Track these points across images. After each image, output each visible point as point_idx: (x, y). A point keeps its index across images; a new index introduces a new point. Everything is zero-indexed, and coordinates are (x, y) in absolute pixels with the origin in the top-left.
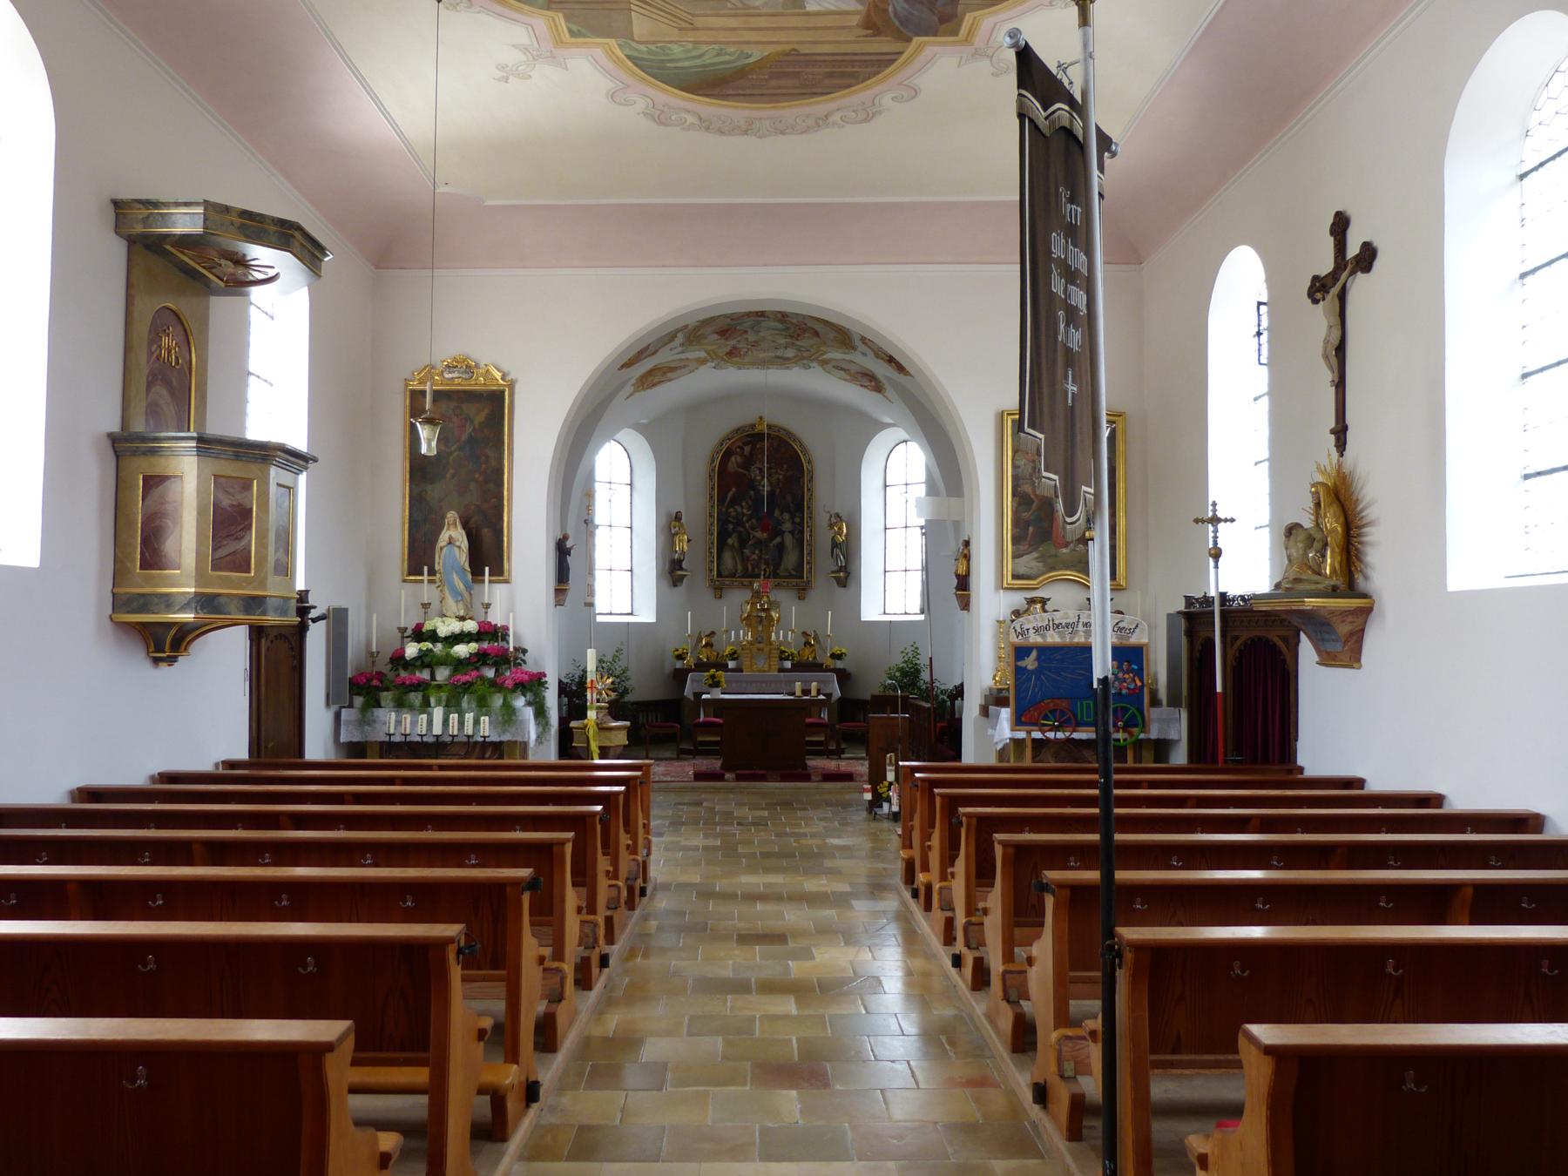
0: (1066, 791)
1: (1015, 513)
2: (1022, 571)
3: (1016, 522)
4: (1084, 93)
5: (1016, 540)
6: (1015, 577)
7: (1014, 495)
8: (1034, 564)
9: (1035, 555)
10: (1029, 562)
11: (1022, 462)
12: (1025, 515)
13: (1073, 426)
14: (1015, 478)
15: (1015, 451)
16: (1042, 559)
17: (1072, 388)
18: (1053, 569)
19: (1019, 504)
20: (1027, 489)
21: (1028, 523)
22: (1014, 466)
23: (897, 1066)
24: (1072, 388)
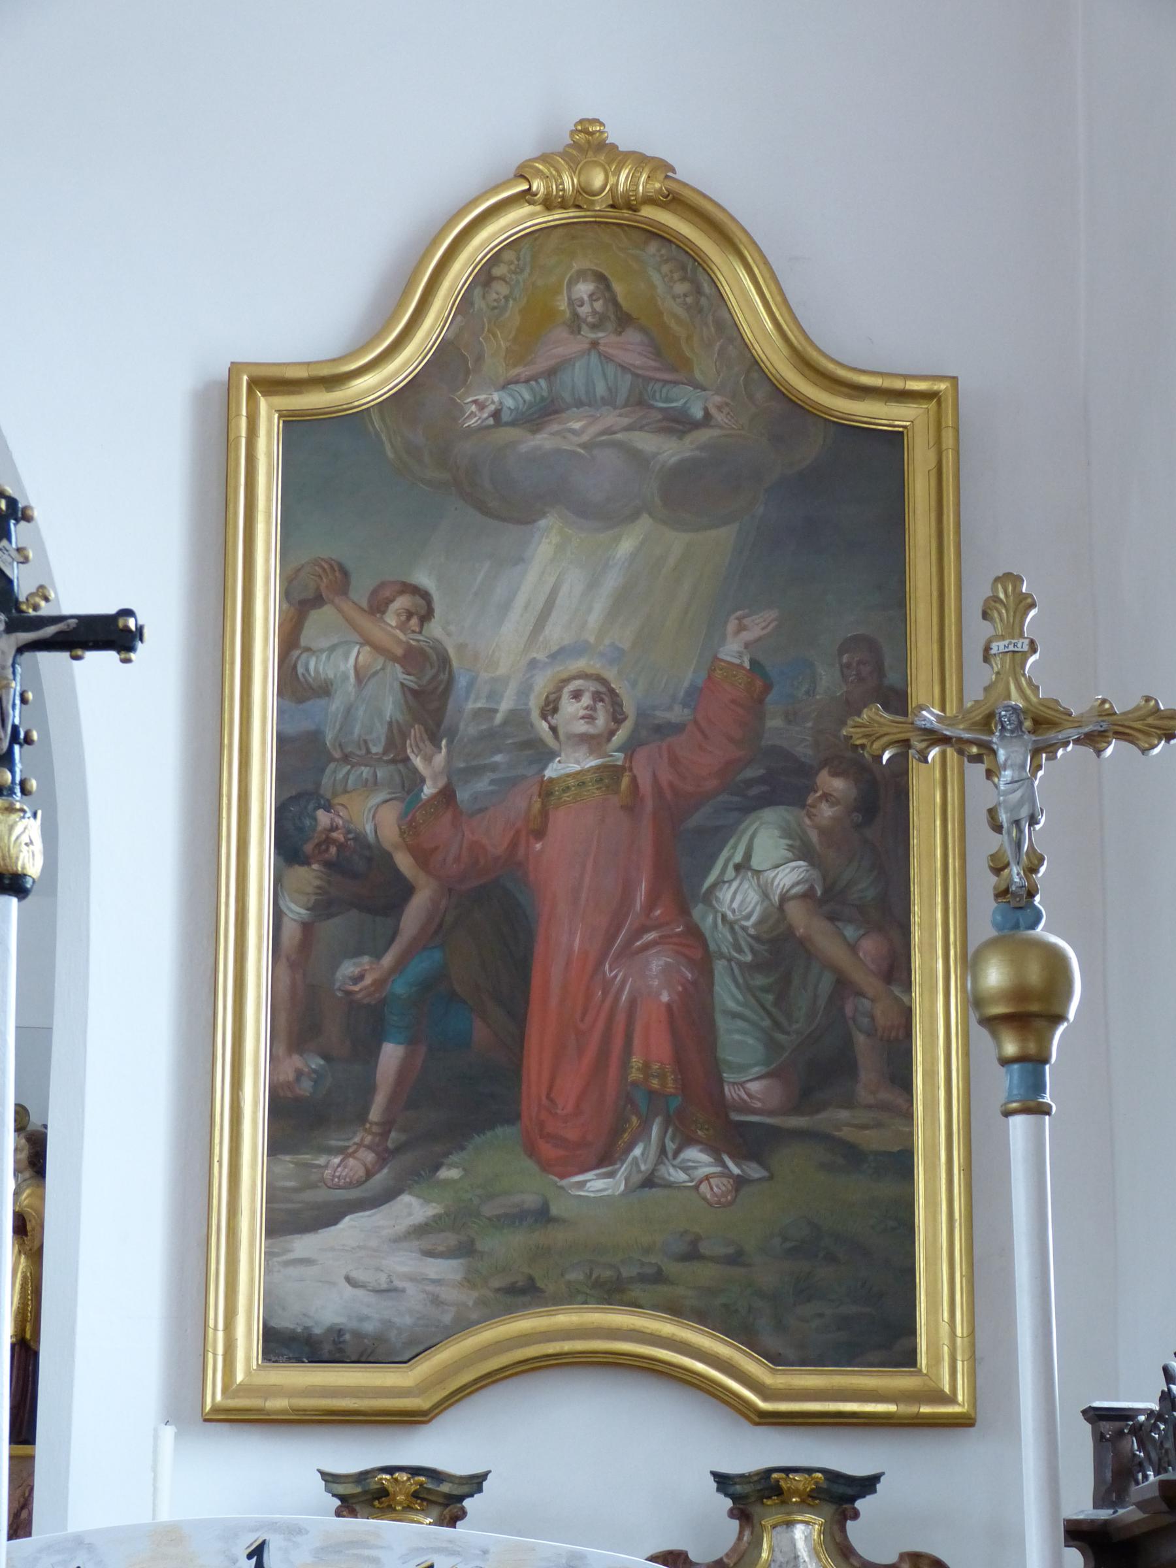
0: (700, 1367)
1: (296, 958)
2: (328, 1307)
3: (303, 1017)
4: (564, 437)
5: (295, 1120)
6: (281, 1344)
7: (289, 848)
8: (404, 1263)
9: (412, 1209)
10: (373, 1259)
11: (338, 661)
12: (357, 973)
13: (959, 493)
14: (300, 757)
15: (300, 604)
16: (454, 1233)
17: (886, 756)
18: (523, 1293)
19: (324, 907)
20: (372, 815)
21: (368, 1023)
22: (294, 686)
23: (324, 643)
24: (886, 756)
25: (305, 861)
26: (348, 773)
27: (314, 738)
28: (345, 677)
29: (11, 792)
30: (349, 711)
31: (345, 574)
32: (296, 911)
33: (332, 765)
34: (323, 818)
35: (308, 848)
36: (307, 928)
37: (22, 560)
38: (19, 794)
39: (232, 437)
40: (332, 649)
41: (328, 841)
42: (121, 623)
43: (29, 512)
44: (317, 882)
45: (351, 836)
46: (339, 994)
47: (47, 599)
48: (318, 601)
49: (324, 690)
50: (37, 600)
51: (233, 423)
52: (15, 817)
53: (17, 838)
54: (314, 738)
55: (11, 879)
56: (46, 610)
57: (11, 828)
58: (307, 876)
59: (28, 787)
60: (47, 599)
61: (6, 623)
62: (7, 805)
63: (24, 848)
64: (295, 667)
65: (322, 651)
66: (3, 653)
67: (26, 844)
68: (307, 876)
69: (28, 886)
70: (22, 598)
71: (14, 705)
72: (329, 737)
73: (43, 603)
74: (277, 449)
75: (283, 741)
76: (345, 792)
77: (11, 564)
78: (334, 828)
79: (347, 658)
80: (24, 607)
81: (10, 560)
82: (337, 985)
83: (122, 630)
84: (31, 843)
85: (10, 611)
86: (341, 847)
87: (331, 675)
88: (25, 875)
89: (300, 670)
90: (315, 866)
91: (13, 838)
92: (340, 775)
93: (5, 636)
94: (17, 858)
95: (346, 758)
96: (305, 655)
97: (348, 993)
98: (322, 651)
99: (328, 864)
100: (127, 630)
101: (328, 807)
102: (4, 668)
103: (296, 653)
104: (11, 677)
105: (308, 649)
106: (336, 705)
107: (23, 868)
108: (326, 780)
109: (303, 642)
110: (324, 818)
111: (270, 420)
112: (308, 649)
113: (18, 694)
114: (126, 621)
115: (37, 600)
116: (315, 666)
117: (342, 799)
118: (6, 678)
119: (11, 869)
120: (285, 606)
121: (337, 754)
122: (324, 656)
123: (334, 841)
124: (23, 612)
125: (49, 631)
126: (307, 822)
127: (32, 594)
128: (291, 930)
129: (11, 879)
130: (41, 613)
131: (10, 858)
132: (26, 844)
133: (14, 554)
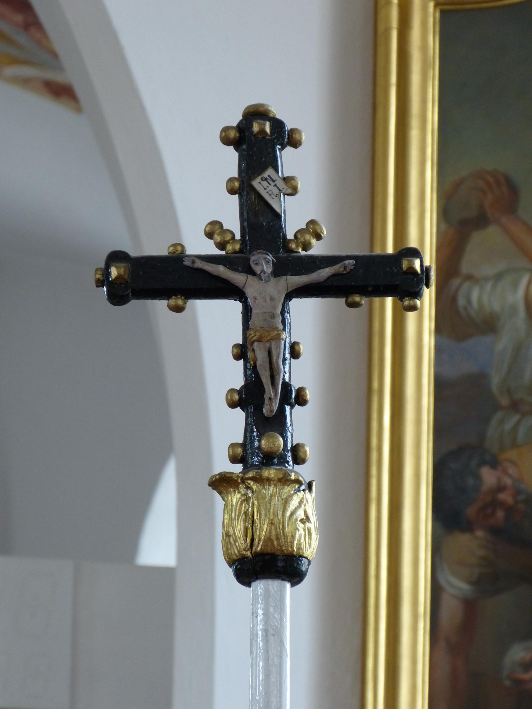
7: (448, 514)
19: (489, 581)
23: (488, 270)
25: (467, 527)
26: (518, 424)
27: (477, 382)
28: (514, 310)
29: (283, 461)
30: (518, 350)
31: (513, 190)
32: (457, 585)
33: (499, 415)
34: (489, 477)
35: (471, 511)
36: (470, 606)
37: (289, 191)
38: (291, 463)
39: (381, 28)
40: (498, 277)
41: (495, 504)
42: (405, 265)
43: (296, 136)
44: (481, 552)
45: (521, 497)
46: (507, 683)
47: (318, 237)
48: (481, 221)
49: (489, 325)
50: (308, 237)
51: (382, 14)
52: (288, 489)
53: (292, 514)
54: (477, 382)
55: (285, 561)
56: (317, 249)
57: (286, 502)
58: (469, 545)
59: (301, 454)
60: (318, 237)
61: (274, 264)
62: (281, 476)
63: (301, 526)
64: (454, 300)
65: (486, 279)
66: (272, 299)
67: (302, 521)
68: (469, 545)
69: (304, 569)
70: (290, 235)
71: (284, 359)
72: (495, 381)
73: (314, 241)
74: (433, 43)
75: (441, 386)
76: (515, 445)
77: (278, 196)
78: (500, 488)
79: (515, 285)
80: (293, 246)
81: (276, 191)
82: (505, 673)
83: (405, 273)
84: (308, 519)
85: (279, 252)
86: (509, 510)
87: (497, 307)
88: (301, 556)
89: (461, 302)
90: (480, 533)
91: (288, 514)
92: (508, 426)
93: (273, 280)
94: (293, 537)
95: (515, 406)
96: (466, 285)
97: (519, 682)
98: (486, 279)
99: (495, 532)
100: (412, 271)
101: (494, 464)
102: (273, 316)
103: (455, 282)
104: (281, 327)
105: (470, 278)
106: (503, 343)
107: (299, 548)
108: (492, 432)
109: (465, 268)
110: (489, 477)
111: (425, 9)
112: (470, 278)
113: (287, 346)
114: (412, 263)
115: (308, 237)
116: (478, 298)
117: (512, 454)
118: (276, 328)
119: (287, 549)
120: (443, 226)
121: (504, 401)
122: (488, 286)
123: (501, 504)
124: (292, 251)
125: (324, 273)
126: (470, 481)
127: (300, 231)
128: (451, 607)
129: (285, 561)
130: (311, 252)
131: (285, 536)
132: (302, 521)
133: (281, 184)
